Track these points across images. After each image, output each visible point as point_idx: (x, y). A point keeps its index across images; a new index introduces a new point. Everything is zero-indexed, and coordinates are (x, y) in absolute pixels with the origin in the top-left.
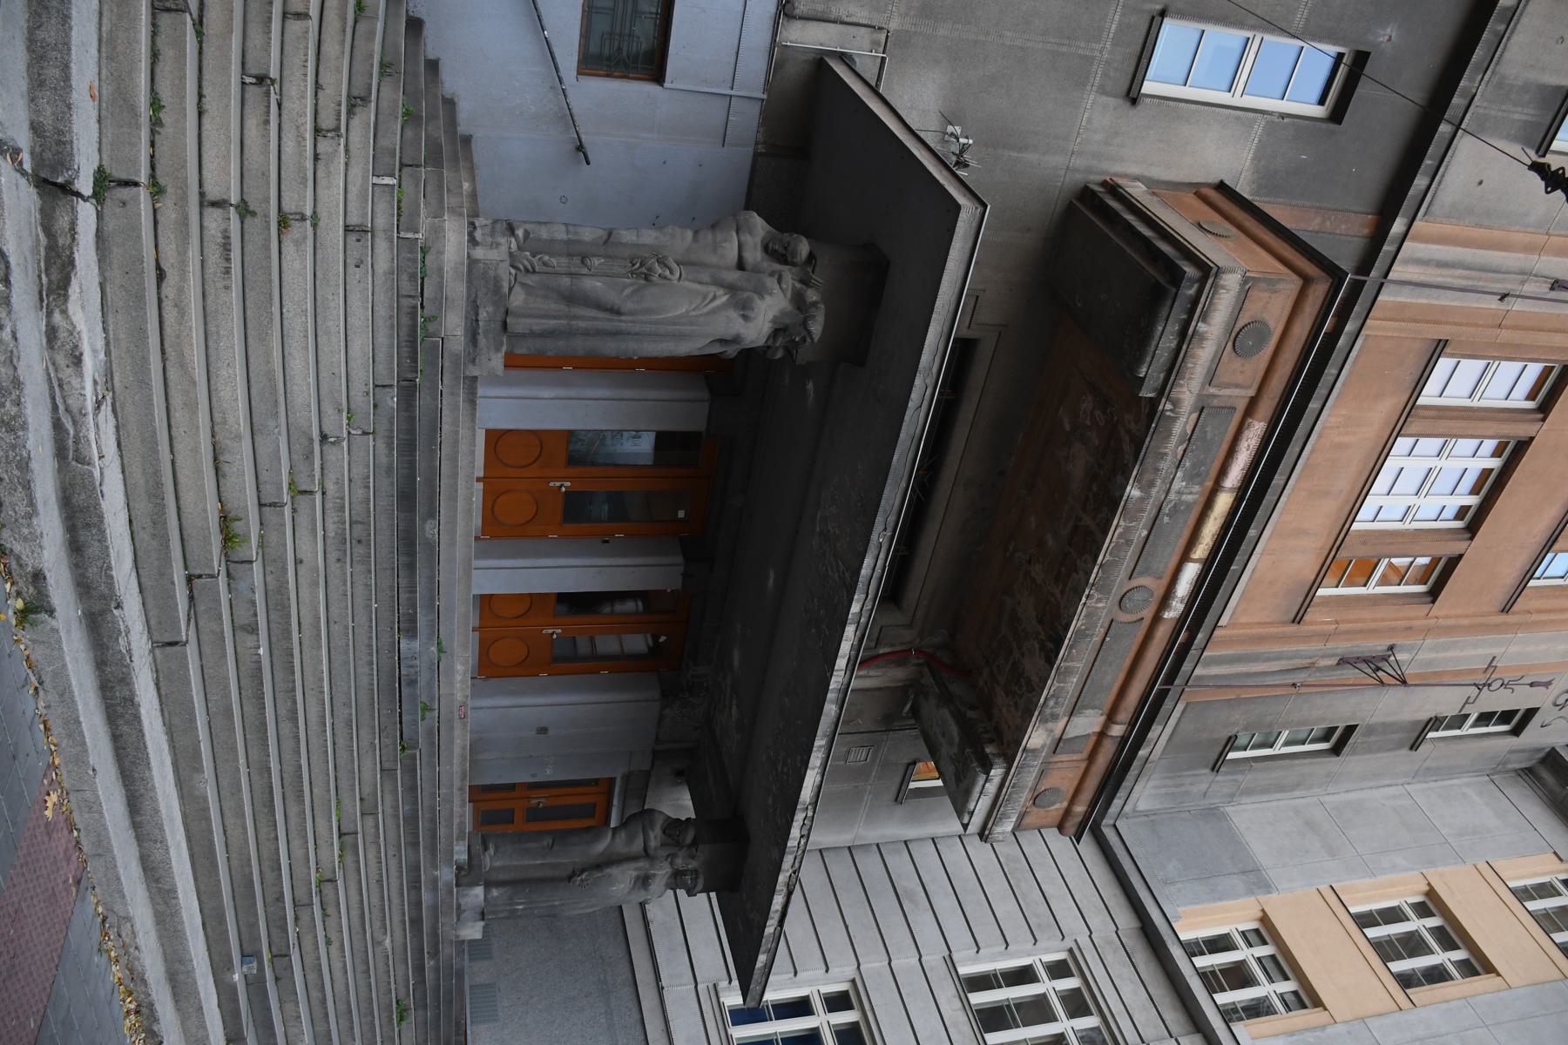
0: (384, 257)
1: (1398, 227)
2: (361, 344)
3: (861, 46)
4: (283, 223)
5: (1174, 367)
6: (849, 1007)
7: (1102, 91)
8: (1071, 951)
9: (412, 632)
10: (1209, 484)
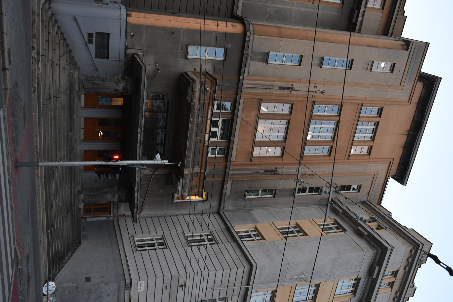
0: (67, 73)
1: (241, 77)
2: (64, 82)
3: (139, 52)
4: (56, 65)
5: (192, 97)
6: (163, 245)
7: (181, 57)
8: (211, 232)
9: (71, 132)
10: (206, 119)
